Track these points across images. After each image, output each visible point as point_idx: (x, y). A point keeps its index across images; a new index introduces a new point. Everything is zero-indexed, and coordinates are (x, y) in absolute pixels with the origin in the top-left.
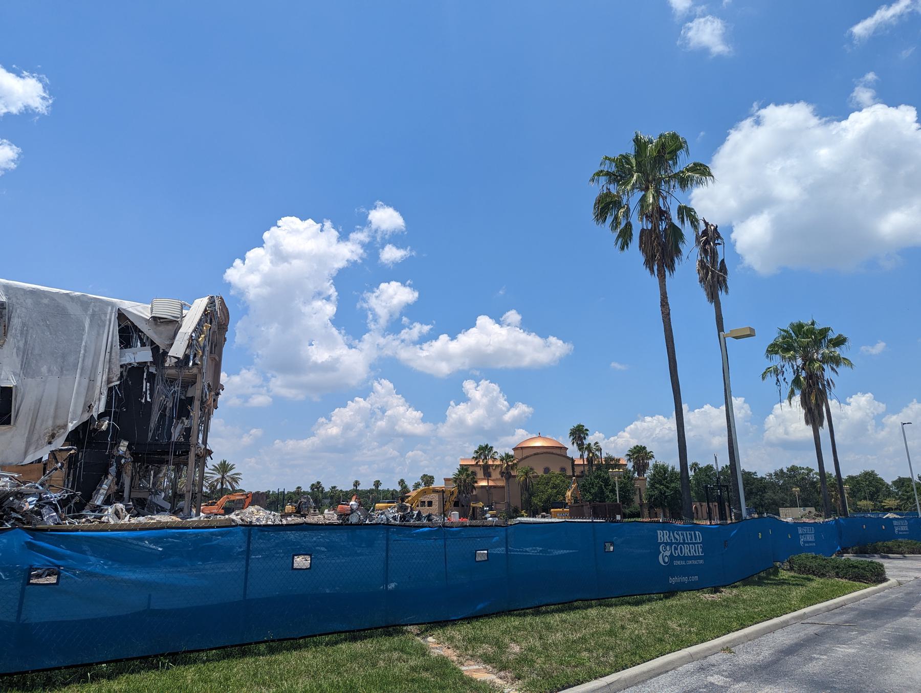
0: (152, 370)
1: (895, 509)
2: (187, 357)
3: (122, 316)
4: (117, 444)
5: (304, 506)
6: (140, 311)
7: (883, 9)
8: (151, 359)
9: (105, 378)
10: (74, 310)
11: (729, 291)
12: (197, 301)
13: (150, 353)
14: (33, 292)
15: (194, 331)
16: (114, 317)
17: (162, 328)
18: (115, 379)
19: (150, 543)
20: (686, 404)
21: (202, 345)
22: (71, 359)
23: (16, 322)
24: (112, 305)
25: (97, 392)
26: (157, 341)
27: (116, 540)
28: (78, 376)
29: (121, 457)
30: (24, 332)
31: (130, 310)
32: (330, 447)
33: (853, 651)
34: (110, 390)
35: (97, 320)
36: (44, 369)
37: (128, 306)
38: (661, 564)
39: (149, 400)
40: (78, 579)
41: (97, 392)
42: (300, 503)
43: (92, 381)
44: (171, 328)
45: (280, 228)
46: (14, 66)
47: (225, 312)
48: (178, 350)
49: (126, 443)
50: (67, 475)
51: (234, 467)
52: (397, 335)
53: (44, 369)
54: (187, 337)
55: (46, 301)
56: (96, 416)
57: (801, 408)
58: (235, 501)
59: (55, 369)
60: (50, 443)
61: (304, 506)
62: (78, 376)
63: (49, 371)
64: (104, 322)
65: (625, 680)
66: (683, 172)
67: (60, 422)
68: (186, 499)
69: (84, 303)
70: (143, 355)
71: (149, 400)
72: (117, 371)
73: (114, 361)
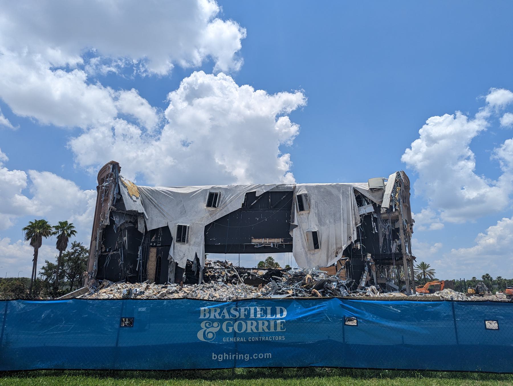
0: (375, 216)
2: (391, 207)
3: (355, 191)
4: (365, 256)
6: (363, 187)
8: (373, 211)
9: (354, 222)
10: (334, 192)
14: (317, 187)
17: (376, 194)
18: (359, 222)
22: (338, 216)
23: (313, 202)
24: (350, 186)
25: (352, 230)
26: (375, 201)
28: (342, 223)
29: (369, 262)
30: (317, 206)
31: (359, 187)
34: (357, 228)
36: (327, 222)
37: (357, 185)
41: (352, 230)
42: (478, 287)
43: (349, 225)
44: (380, 192)
53: (327, 222)
55: (322, 190)
56: (354, 242)
59: (332, 221)
60: (336, 256)
63: (330, 222)
64: (348, 195)
67: (339, 246)
70: (369, 209)
72: (359, 218)
73: (356, 213)
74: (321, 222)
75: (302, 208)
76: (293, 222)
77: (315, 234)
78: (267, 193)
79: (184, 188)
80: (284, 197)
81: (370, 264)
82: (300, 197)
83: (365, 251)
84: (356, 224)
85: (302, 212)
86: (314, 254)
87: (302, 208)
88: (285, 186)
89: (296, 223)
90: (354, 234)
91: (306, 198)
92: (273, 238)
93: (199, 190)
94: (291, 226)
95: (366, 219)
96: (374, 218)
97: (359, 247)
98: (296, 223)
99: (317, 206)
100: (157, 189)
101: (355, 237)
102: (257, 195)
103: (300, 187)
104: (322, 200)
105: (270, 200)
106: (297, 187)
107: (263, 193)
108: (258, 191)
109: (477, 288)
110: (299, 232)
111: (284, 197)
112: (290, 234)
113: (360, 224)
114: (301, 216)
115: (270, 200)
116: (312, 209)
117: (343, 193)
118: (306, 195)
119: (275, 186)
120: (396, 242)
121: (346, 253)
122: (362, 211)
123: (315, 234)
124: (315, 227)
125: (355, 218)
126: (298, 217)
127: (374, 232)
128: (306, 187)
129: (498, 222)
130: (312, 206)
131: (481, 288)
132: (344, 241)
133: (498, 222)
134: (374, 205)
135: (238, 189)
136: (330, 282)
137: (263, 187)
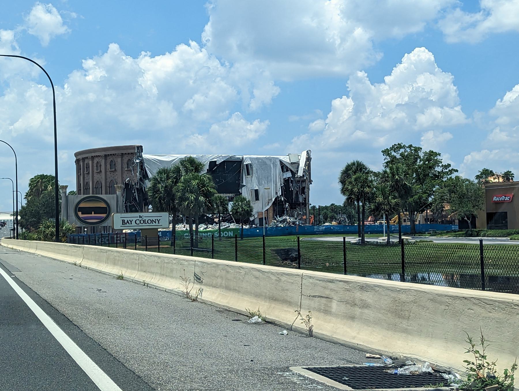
0: (292, 179)
2: (303, 176)
3: (281, 162)
4: (285, 204)
5: (342, 222)
6: (286, 159)
8: (291, 176)
9: (280, 184)
10: (268, 162)
12: (303, 153)
13: (291, 174)
14: (257, 158)
15: (305, 166)
16: (279, 163)
17: (294, 165)
18: (282, 183)
21: (451, 385)
22: (270, 178)
23: (254, 169)
24: (278, 158)
25: (278, 188)
26: (293, 170)
28: (272, 184)
29: (287, 208)
30: (257, 172)
31: (283, 160)
34: (281, 187)
35: (275, 166)
36: (263, 182)
37: (282, 158)
39: (292, 189)
41: (278, 188)
42: (341, 220)
43: (276, 185)
44: (297, 165)
48: (300, 173)
49: (288, 204)
50: (417, 289)
53: (263, 182)
54: (303, 169)
55: (260, 161)
56: (279, 196)
59: (266, 182)
60: (268, 205)
61: (342, 222)
62: (272, 184)
63: (265, 183)
64: (276, 165)
67: (270, 198)
69: (270, 159)
70: (289, 175)
71: (292, 189)
72: (282, 181)
73: (281, 178)
74: (259, 184)
75: (248, 174)
76: (242, 183)
77: (256, 191)
78: (224, 162)
79: (165, 157)
80: (235, 165)
81: (288, 209)
82: (247, 165)
83: (286, 202)
84: (281, 185)
85: (248, 176)
86: (254, 204)
87: (248, 174)
88: (236, 157)
89: (244, 184)
90: (279, 191)
91: (251, 167)
92: (228, 193)
93: (176, 159)
94: (240, 185)
95: (287, 181)
96: (291, 180)
97: (282, 200)
98: (244, 184)
99: (257, 172)
100: (148, 158)
101: (280, 193)
102: (217, 163)
103: (246, 158)
104: (260, 168)
105: (225, 167)
106: (244, 158)
107: (221, 162)
108: (218, 160)
109: (340, 221)
110: (246, 189)
111: (235, 165)
112: (240, 190)
113: (283, 185)
114: (247, 179)
115: (225, 167)
116: (254, 174)
117: (273, 163)
118: (251, 165)
119: (229, 157)
120: (302, 195)
121: (274, 203)
122: (285, 176)
123: (256, 191)
124: (256, 186)
125: (281, 180)
126: (245, 180)
127: (290, 190)
128: (250, 158)
129: (68, 76)
130: (254, 172)
131: (343, 221)
132: (273, 195)
133: (68, 76)
134: (292, 171)
135: (204, 158)
136: (296, 222)
137: (221, 157)
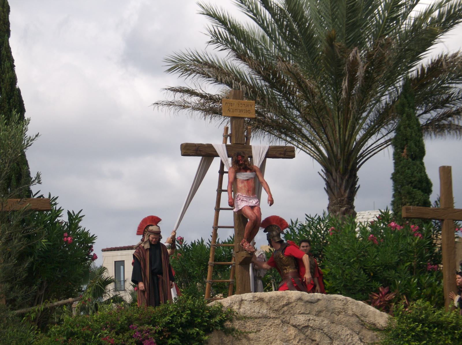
1: (188, 107)
7: (425, 136)
11: (324, 189)
19: (174, 315)
20: (231, 158)
27: (324, 143)
32: (34, 244)
33: (243, 47)
38: (422, 168)
40: (350, 121)
45: (224, 163)
46: (309, 3)
47: (156, 281)
51: (61, 209)
52: (116, 295)
57: (201, 92)
58: (230, 292)
65: (250, 139)
66: (347, 7)
68: (151, 309)
